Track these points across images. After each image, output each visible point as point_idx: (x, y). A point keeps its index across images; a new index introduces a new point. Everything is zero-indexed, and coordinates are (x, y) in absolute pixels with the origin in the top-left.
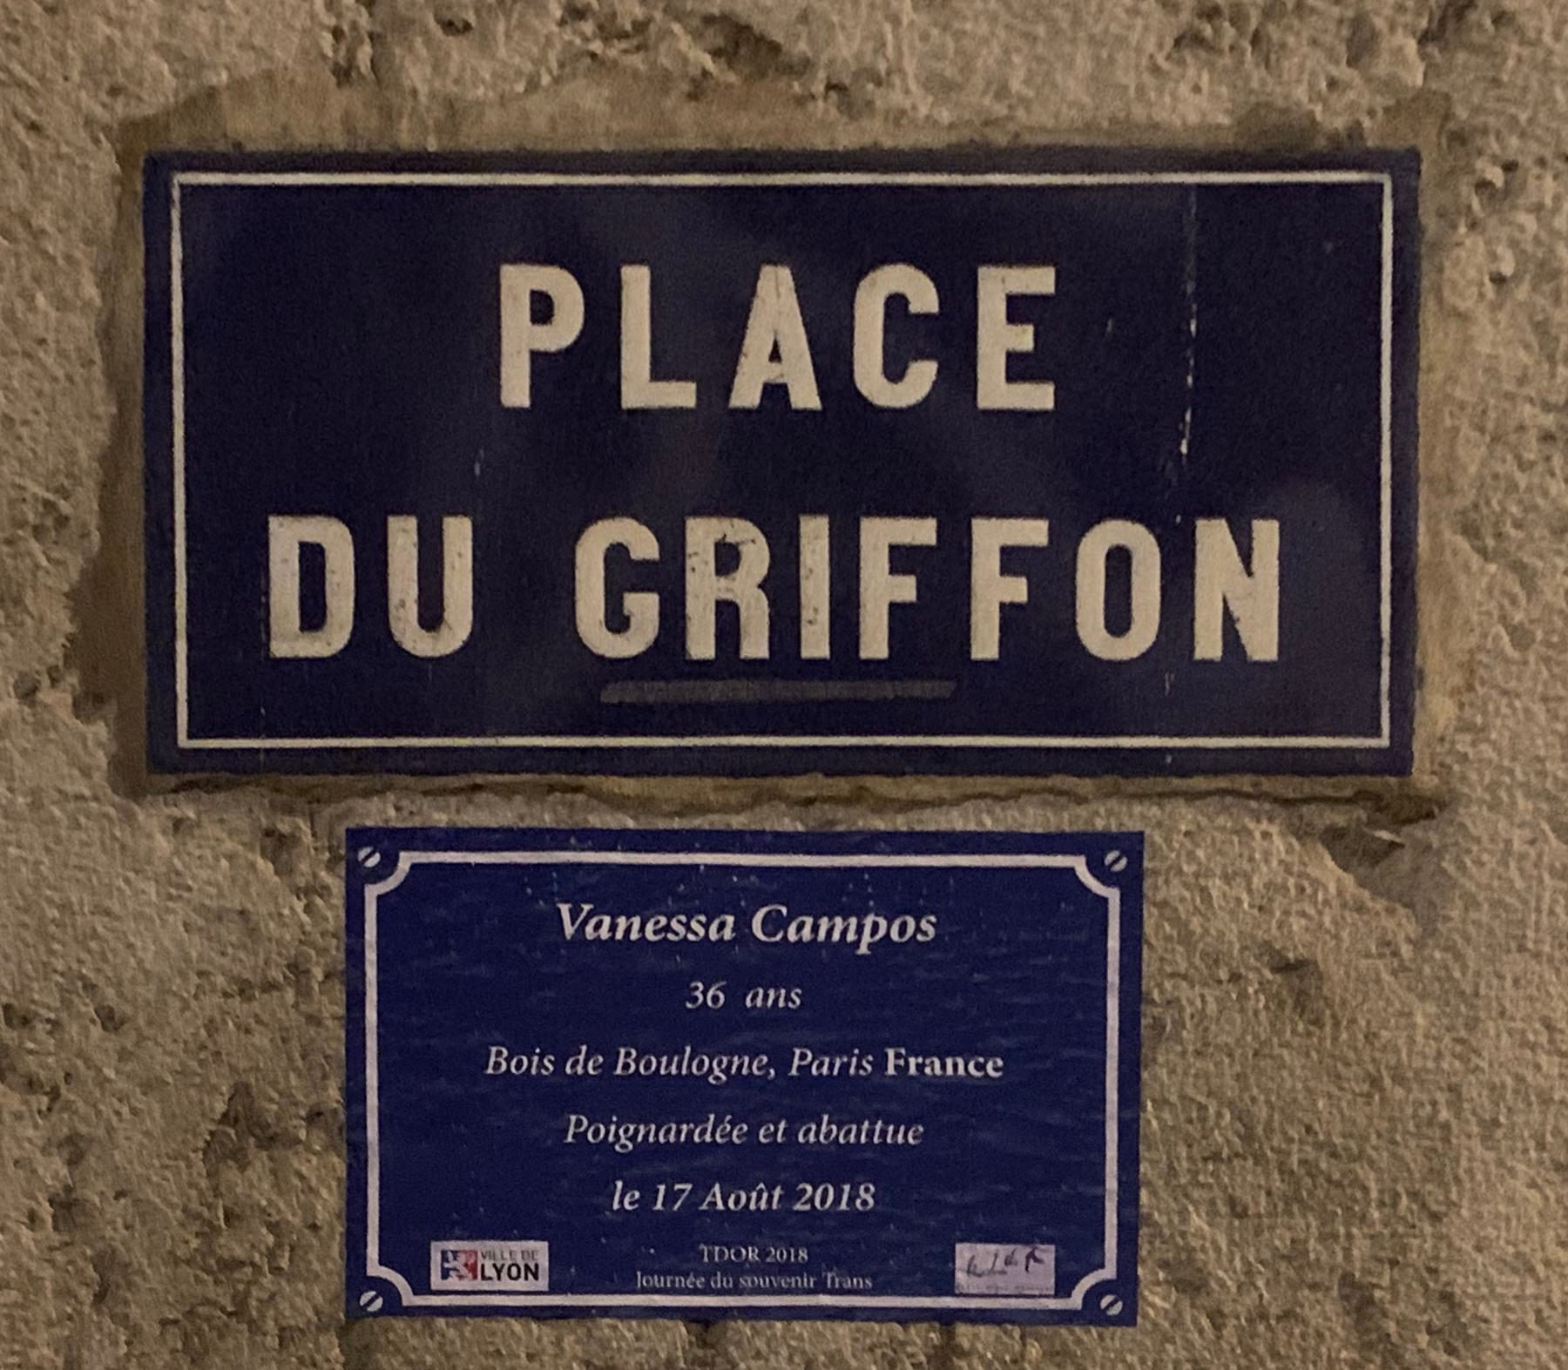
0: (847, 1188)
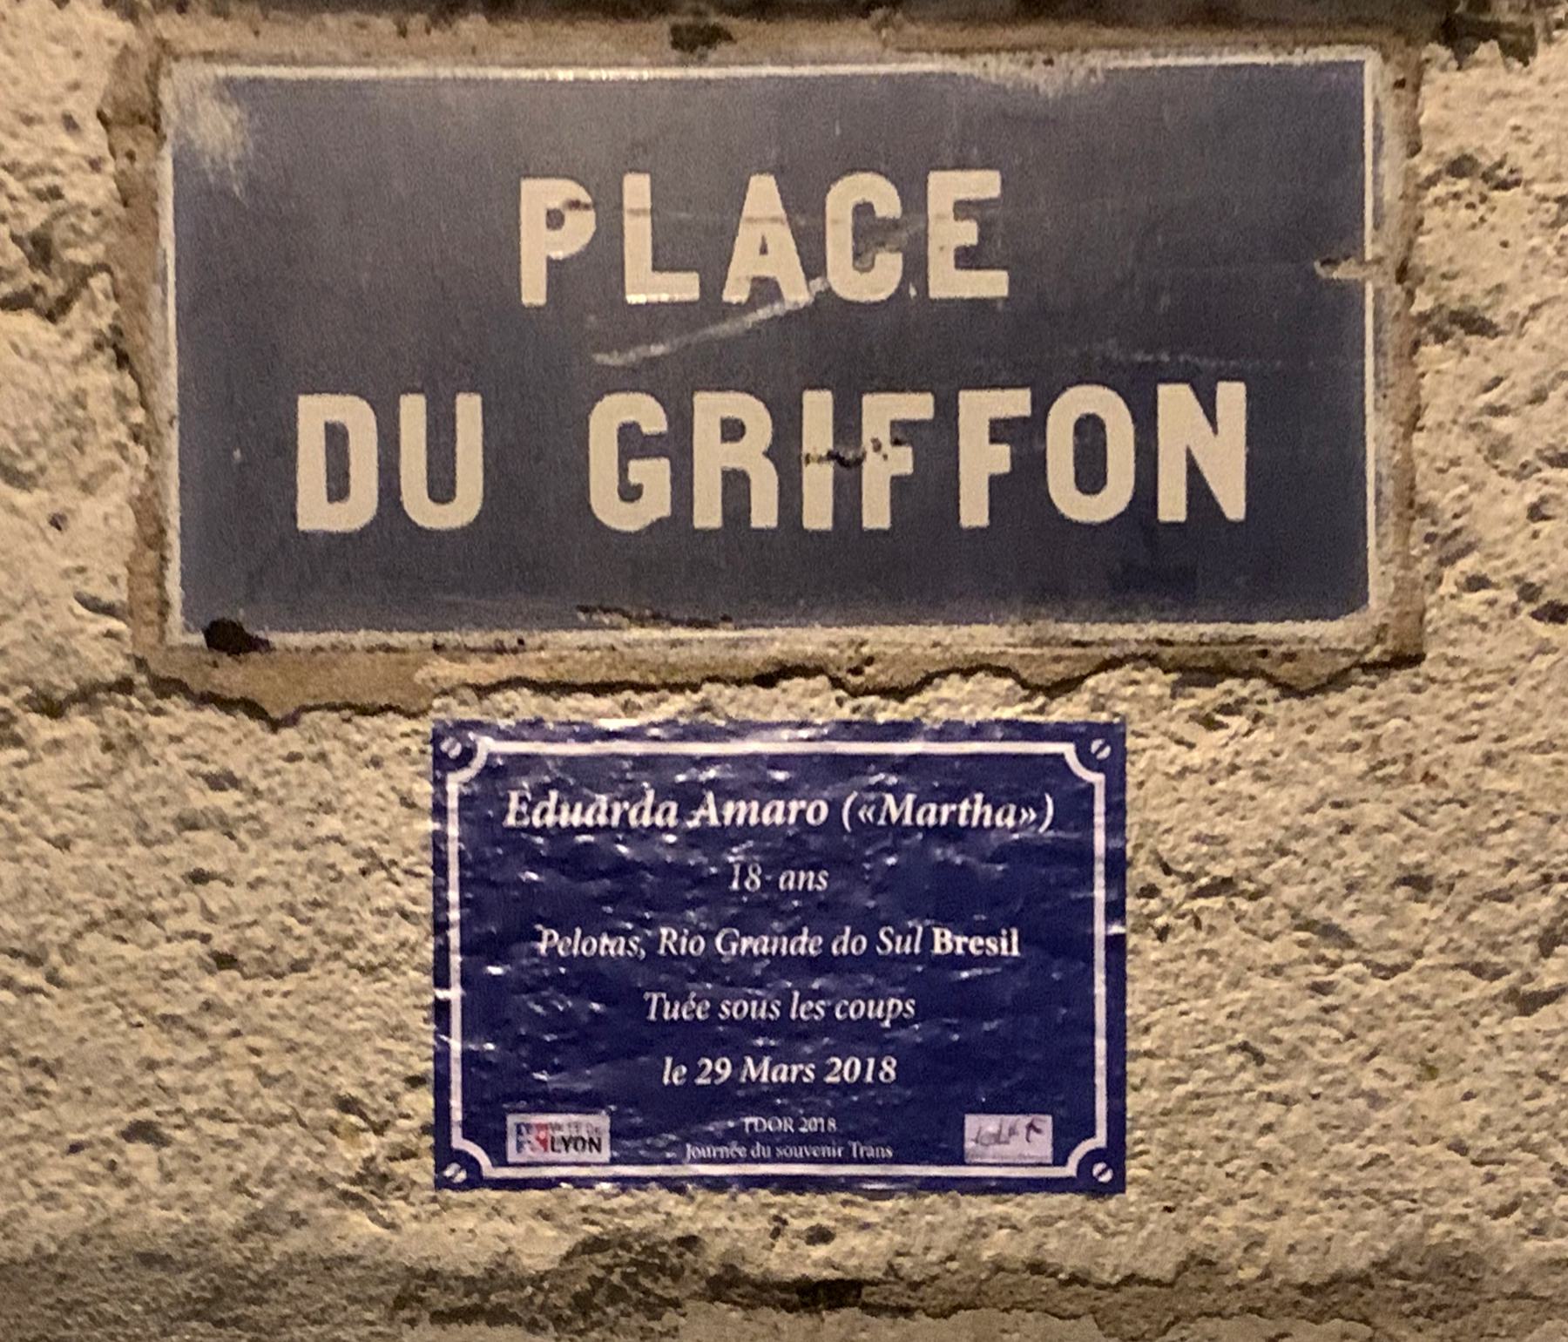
0: (871, 1062)
